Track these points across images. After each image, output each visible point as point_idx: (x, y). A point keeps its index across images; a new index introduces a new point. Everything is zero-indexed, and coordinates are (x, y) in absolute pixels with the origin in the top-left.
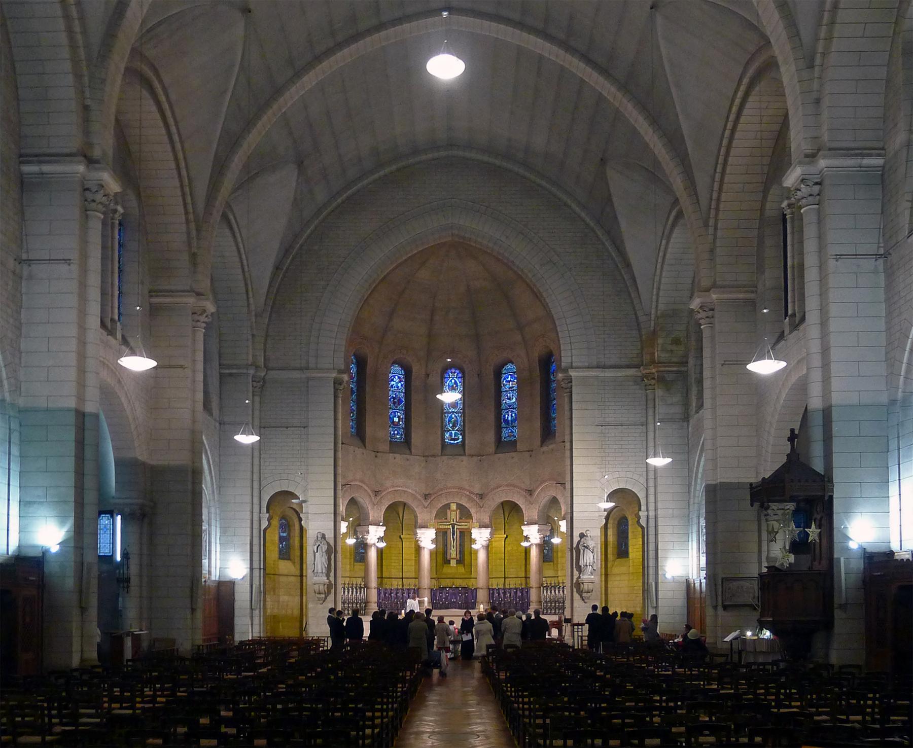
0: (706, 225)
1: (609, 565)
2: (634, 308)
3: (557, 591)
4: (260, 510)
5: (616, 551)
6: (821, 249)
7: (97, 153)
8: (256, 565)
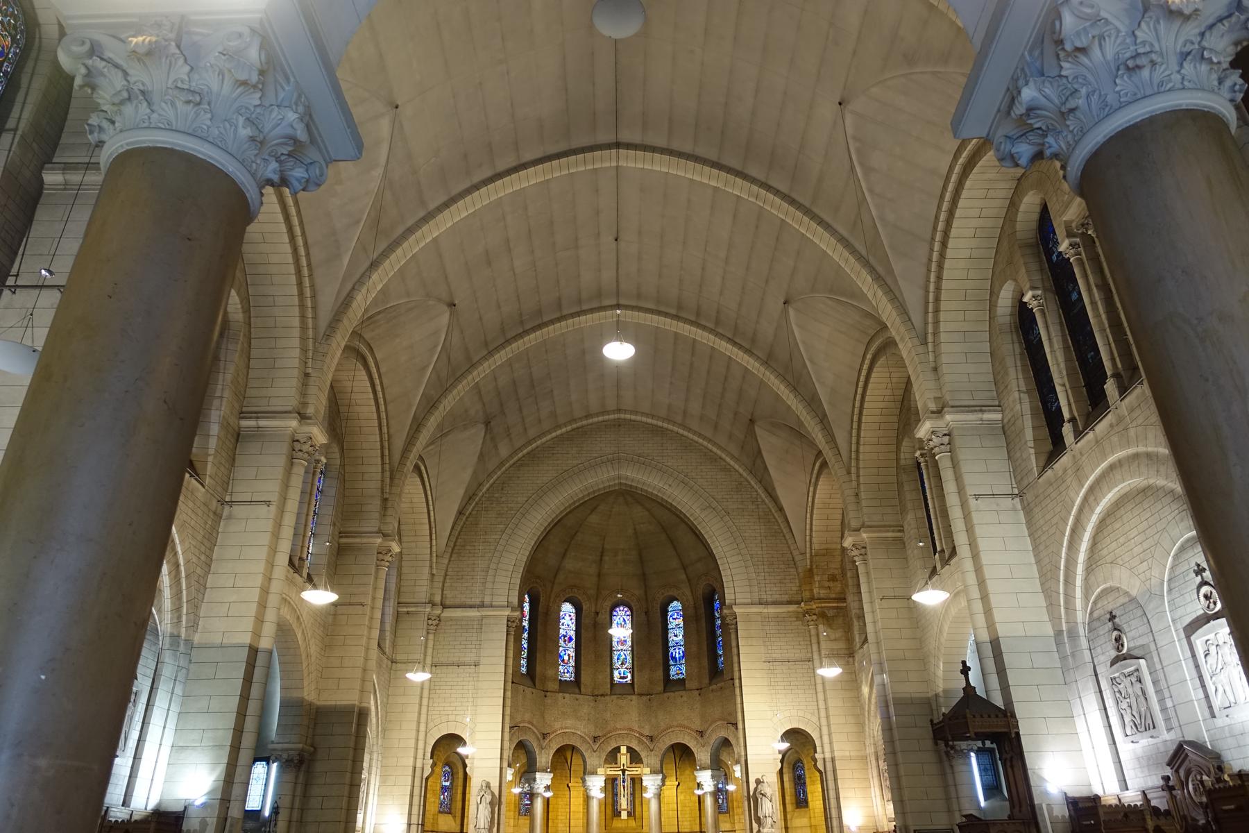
1: (789, 817)
2: (789, 547)
6: (961, 490)
7: (310, 411)
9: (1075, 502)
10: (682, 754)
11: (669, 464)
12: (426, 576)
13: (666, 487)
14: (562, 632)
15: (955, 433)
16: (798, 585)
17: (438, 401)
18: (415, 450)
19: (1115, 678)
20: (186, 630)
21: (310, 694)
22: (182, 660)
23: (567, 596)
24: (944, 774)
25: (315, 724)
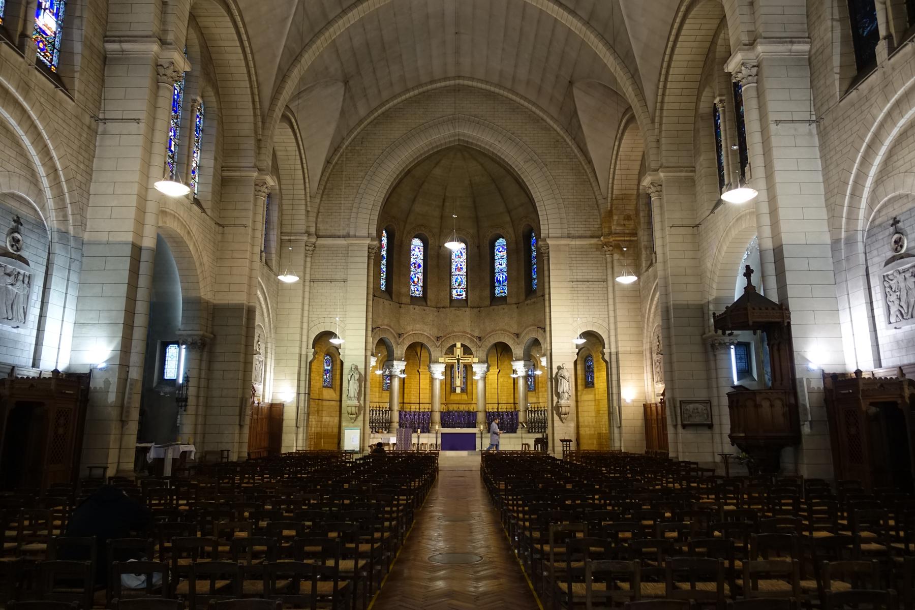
0: (653, 122)
1: (579, 394)
2: (594, 193)
3: (539, 414)
4: (307, 346)
5: (584, 383)
7: (170, 37)
8: (302, 390)
9: (877, 118)
10: (502, 351)
11: (499, 124)
12: (304, 212)
13: (497, 143)
14: (413, 260)
15: (764, 64)
16: (599, 223)
17: (300, 55)
18: (282, 98)
19: (887, 276)
20: (74, 229)
21: (206, 293)
22: (73, 253)
23: (417, 233)
24: (707, 361)
25: (213, 317)
